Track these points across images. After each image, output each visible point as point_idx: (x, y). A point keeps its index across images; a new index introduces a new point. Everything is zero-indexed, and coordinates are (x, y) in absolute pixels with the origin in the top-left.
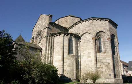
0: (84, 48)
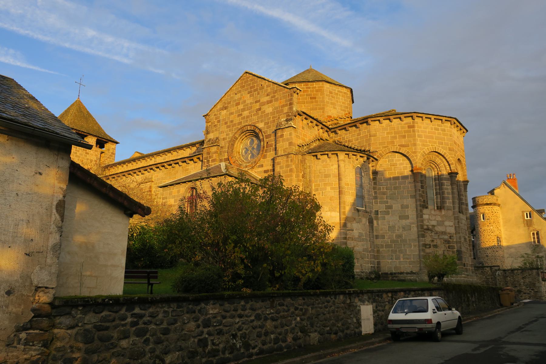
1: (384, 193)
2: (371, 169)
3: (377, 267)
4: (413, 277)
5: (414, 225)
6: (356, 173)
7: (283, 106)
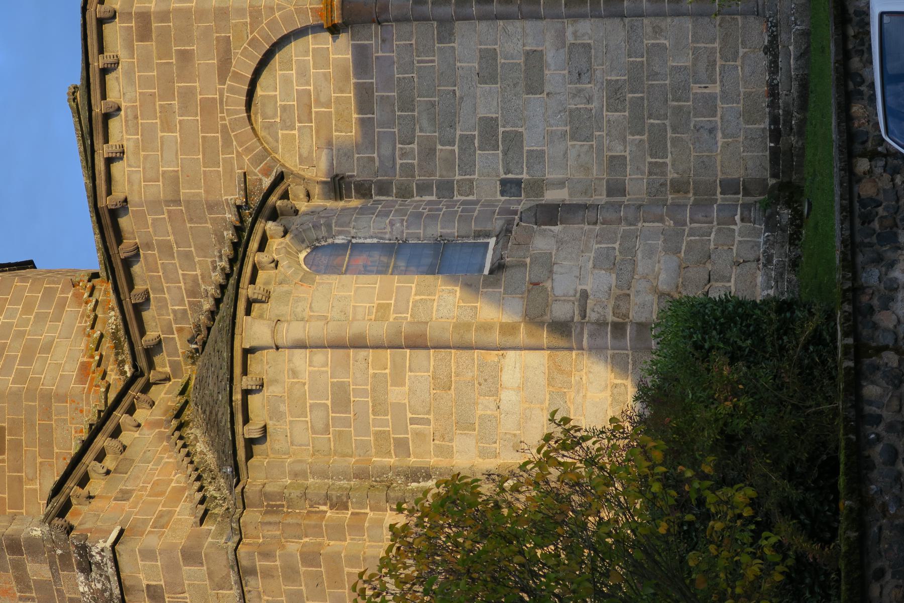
0: (424, 131)
1: (429, 153)
2: (318, 202)
3: (747, 193)
4: (791, 47)
5: (569, 31)
6: (335, 269)
7: (22, 580)
